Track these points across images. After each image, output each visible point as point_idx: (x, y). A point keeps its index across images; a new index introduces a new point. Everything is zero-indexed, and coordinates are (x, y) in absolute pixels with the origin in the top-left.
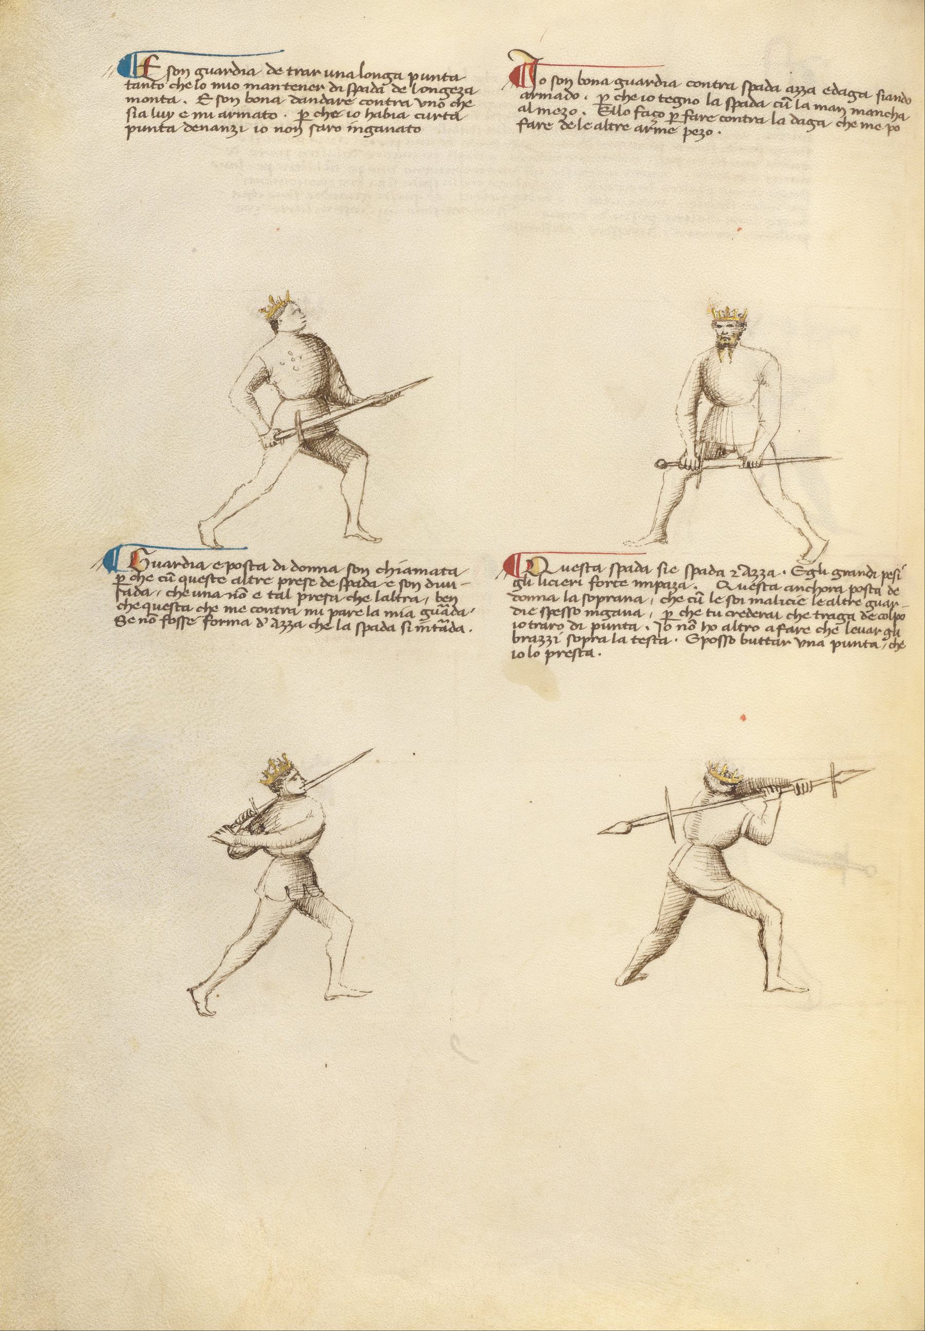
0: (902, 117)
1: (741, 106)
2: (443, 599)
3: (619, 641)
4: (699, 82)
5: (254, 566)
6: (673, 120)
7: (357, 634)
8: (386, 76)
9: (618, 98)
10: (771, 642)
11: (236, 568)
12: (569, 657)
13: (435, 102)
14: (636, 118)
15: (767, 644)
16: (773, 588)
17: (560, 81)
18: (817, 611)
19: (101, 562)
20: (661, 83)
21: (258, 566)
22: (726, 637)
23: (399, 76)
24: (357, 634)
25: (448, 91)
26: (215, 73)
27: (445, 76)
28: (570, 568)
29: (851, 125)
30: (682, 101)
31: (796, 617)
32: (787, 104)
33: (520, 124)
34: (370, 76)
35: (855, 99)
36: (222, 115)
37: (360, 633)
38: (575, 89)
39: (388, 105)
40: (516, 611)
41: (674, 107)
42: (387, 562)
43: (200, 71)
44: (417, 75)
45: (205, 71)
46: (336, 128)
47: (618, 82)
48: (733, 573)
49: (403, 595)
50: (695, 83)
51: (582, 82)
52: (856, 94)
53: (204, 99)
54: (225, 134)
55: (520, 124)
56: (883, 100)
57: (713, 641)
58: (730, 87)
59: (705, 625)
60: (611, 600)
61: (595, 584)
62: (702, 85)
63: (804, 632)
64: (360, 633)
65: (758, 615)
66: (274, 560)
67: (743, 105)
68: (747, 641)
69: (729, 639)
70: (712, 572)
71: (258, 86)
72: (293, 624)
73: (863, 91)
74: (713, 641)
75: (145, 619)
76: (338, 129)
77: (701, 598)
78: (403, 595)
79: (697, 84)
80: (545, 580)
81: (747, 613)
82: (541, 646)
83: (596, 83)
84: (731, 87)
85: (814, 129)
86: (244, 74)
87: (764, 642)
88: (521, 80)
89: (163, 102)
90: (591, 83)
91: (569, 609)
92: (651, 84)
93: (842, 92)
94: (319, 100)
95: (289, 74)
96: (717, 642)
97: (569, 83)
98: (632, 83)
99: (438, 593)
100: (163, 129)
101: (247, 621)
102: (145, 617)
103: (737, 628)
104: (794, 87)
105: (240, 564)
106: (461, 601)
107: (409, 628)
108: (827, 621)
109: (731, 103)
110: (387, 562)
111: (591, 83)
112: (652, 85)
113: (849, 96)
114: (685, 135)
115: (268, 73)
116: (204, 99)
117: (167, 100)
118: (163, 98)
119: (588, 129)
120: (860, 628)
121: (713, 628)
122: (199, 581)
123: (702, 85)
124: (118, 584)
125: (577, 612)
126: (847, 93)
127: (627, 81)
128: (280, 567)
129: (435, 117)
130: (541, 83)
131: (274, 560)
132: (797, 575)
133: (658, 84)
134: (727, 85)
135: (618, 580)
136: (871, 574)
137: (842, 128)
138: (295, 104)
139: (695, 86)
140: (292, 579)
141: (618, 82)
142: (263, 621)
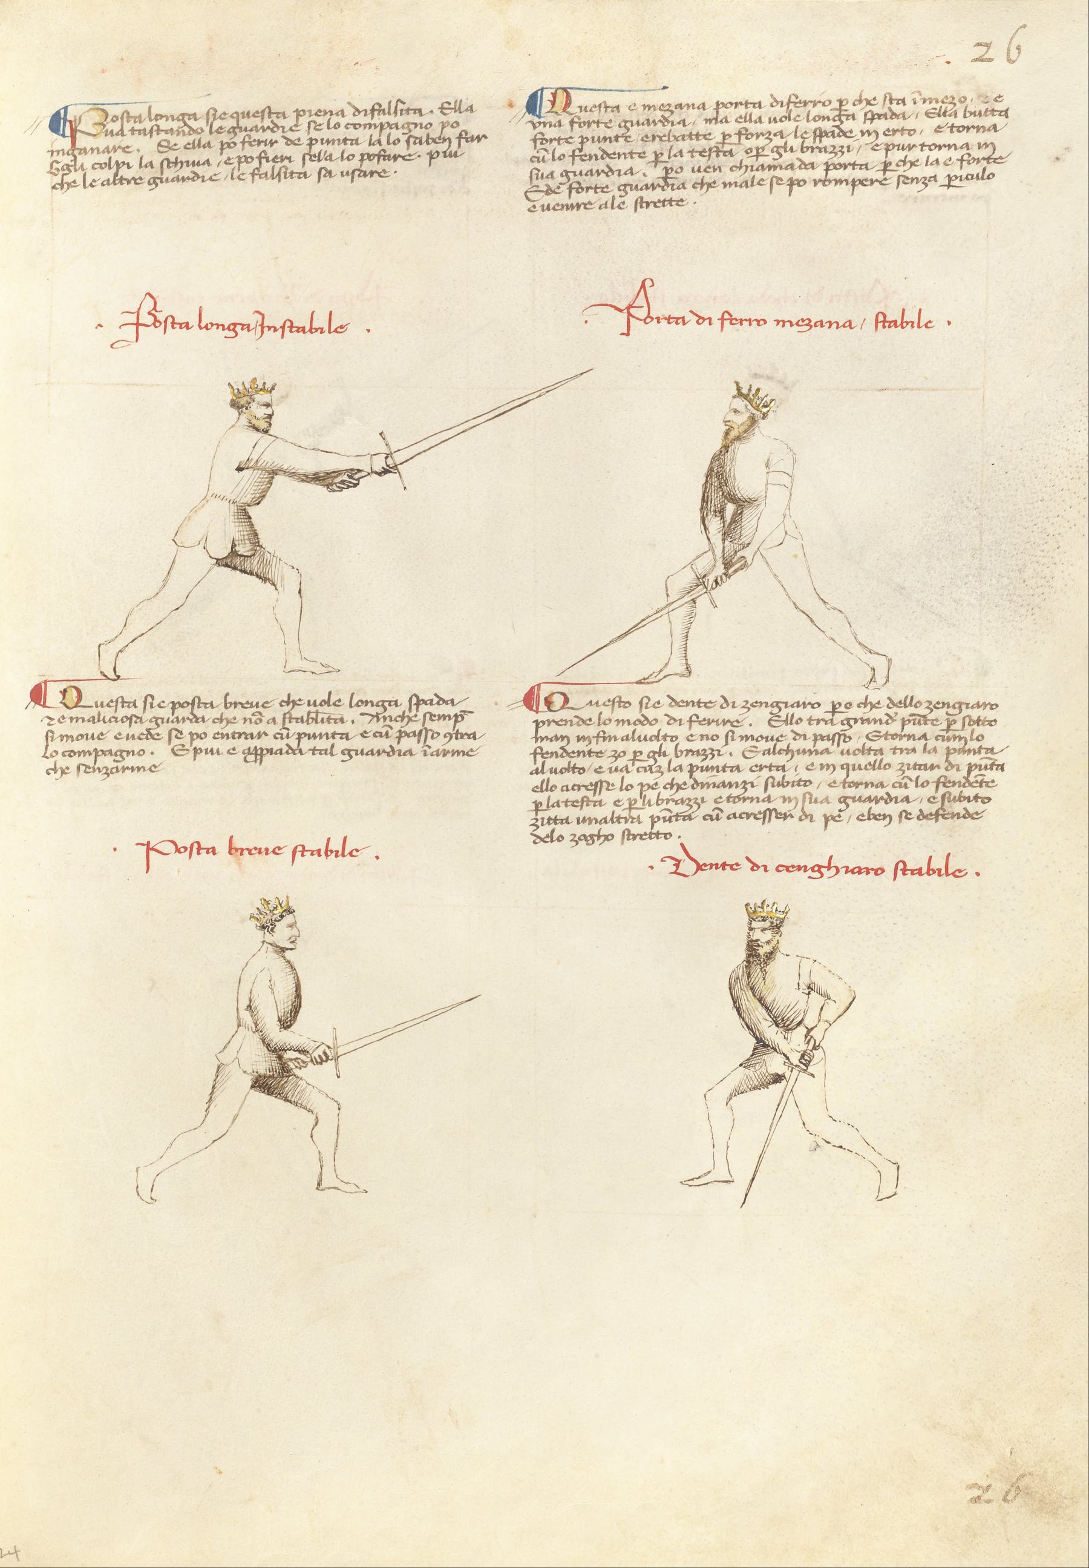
0: (991, 723)
1: (823, 740)
3: (146, 166)
4: (962, 126)
6: (951, 184)
9: (50, 771)
10: (775, 768)
12: (758, 819)
13: (556, 752)
16: (922, 767)
20: (698, 785)
23: (194, 116)
28: (851, 751)
30: (238, 328)
31: (62, 188)
32: (387, 733)
33: (535, 140)
35: (351, 757)
39: (556, 824)
42: (289, 695)
43: (235, 327)
44: (200, 749)
45: (572, 174)
47: (564, 174)
52: (352, 753)
55: (535, 754)
56: (773, 786)
57: (729, 105)
59: (149, 135)
62: (937, 148)
65: (560, 207)
67: (825, 738)
73: (191, 111)
75: (250, 720)
76: (668, 836)
79: (961, 129)
83: (982, 129)
88: (61, 129)
90: (976, 162)
92: (658, 188)
93: (428, 702)
94: (559, 754)
96: (190, 706)
98: (362, 753)
100: (175, 326)
104: (681, 323)
108: (926, 745)
110: (289, 695)
112: (882, 802)
117: (775, 768)
118: (699, 702)
121: (610, 838)
123: (937, 148)
127: (163, 719)
128: (806, 816)
135: (672, 815)
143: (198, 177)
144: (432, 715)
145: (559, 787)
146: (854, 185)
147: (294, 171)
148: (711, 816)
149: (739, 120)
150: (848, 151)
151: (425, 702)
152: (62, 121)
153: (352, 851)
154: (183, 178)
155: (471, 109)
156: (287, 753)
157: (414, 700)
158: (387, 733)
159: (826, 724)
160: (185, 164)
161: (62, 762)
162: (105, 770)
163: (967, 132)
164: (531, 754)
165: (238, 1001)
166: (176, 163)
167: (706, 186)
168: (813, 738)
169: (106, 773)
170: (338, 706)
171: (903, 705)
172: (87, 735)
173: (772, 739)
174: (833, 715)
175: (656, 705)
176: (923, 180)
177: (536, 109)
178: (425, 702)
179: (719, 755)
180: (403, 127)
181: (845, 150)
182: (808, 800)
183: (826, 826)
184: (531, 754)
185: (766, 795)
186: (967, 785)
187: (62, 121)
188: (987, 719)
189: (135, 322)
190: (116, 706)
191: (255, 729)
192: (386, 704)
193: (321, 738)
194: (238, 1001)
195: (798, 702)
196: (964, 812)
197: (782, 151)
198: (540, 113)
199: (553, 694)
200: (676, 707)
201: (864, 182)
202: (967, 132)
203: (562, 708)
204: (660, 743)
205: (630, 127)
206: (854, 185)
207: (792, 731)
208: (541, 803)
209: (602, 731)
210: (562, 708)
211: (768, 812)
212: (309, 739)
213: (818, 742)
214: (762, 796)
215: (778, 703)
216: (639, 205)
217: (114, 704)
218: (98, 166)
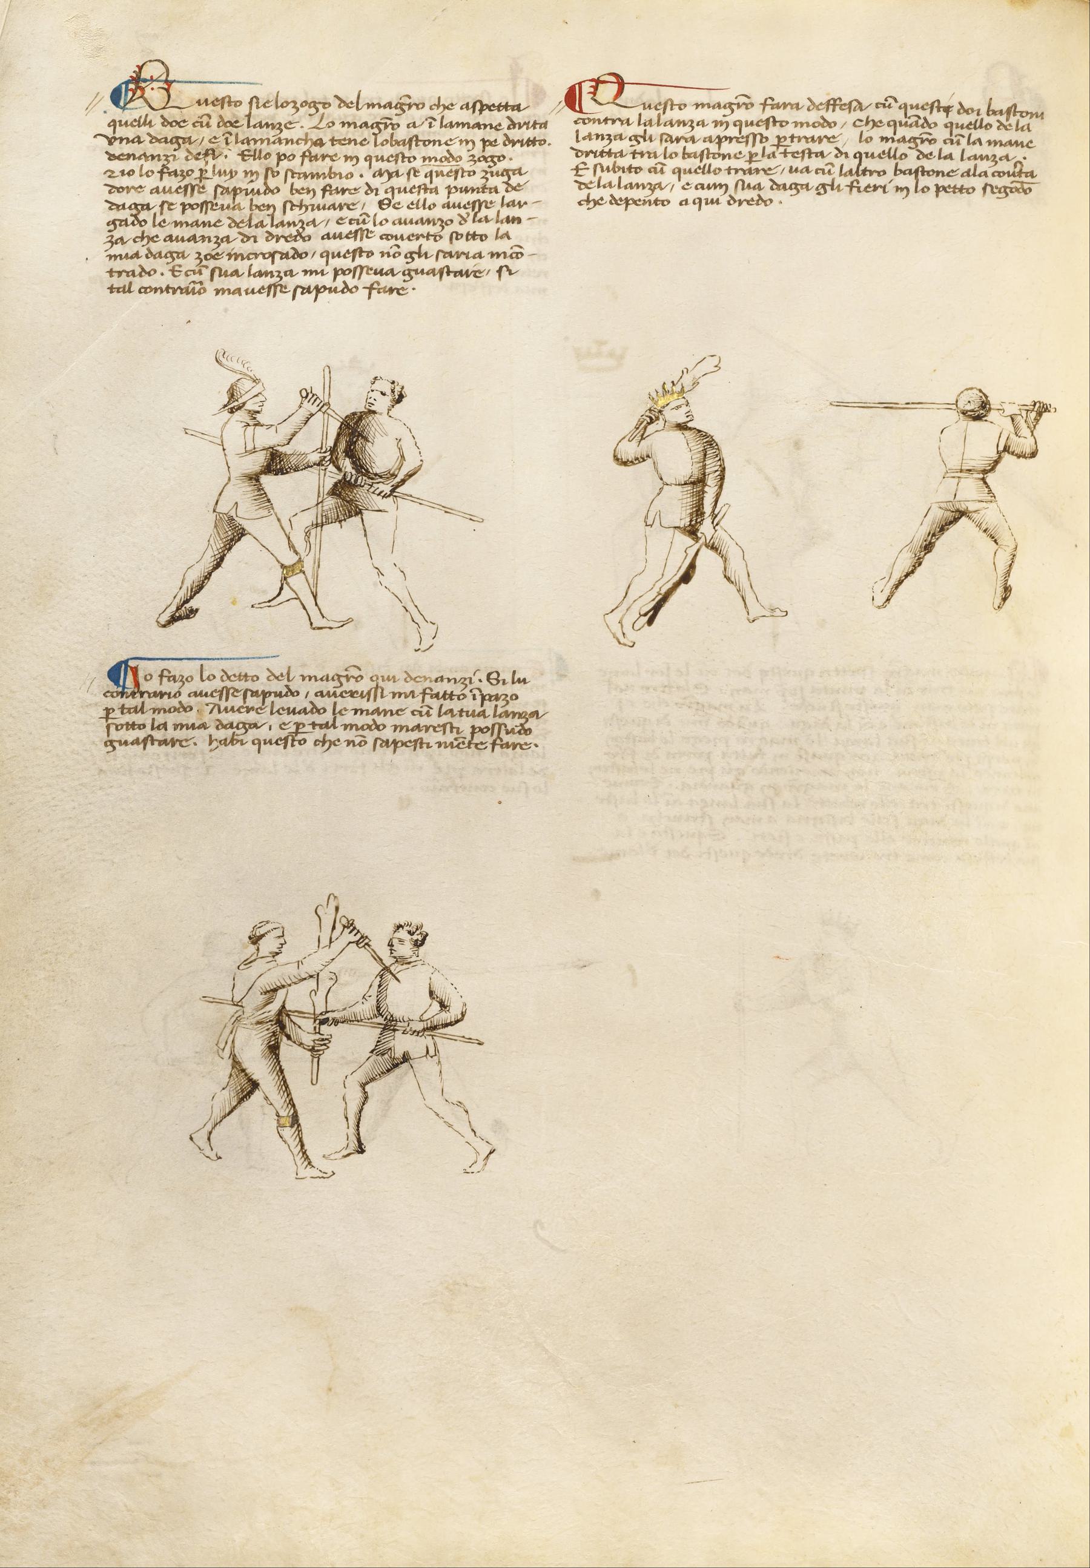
2: (297, 191)
8: (169, 255)
10: (479, 237)
19: (563, 103)
21: (455, 273)
25: (139, 207)
29: (596, 203)
32: (829, 171)
38: (766, 194)
40: (112, 189)
41: (724, 116)
48: (197, 255)
49: (475, 741)
51: (991, 113)
53: (581, 169)
54: (789, 192)
56: (220, 276)
57: (195, 207)
63: (349, 208)
64: (537, 133)
71: (121, 259)
74: (195, 207)
76: (749, 106)
77: (364, 220)
78: (475, 741)
81: (296, 236)
89: (656, 205)
91: (755, 136)
97: (470, 143)
99: (897, 164)
101: (759, 184)
103: (860, 172)
105: (197, 204)
106: (101, 664)
109: (478, 106)
111: (935, 174)
116: (581, 169)
118: (168, 288)
119: (289, 241)
120: (596, 151)
124: (107, 718)
126: (163, 255)
129: (875, 188)
136: (257, 742)
137: (585, 206)
140: (164, 692)
142: (465, 216)
143: (735, 201)
146: (627, 204)
147: (431, 233)
148: (420, 712)
149: (411, 206)
153: (855, 122)
154: (519, 203)
155: (580, 203)
156: (133, 224)
158: (829, 171)
159: (622, 124)
160: (310, 208)
161: (595, 194)
162: (300, 224)
165: (304, 608)
166: (301, 206)
168: (935, 189)
169: (650, 189)
170: (284, 729)
172: (313, 210)
175: (1030, 145)
176: (278, 126)
180: (130, 207)
182: (254, 105)
185: (482, 709)
192: (175, 255)
193: (709, 185)
194: (304, 608)
195: (631, 184)
196: (758, 198)
197: (415, 256)
201: (638, 202)
206: (627, 204)
211: (497, 727)
213: (475, 735)
214: (478, 709)
216: (418, 745)
218: (581, 121)
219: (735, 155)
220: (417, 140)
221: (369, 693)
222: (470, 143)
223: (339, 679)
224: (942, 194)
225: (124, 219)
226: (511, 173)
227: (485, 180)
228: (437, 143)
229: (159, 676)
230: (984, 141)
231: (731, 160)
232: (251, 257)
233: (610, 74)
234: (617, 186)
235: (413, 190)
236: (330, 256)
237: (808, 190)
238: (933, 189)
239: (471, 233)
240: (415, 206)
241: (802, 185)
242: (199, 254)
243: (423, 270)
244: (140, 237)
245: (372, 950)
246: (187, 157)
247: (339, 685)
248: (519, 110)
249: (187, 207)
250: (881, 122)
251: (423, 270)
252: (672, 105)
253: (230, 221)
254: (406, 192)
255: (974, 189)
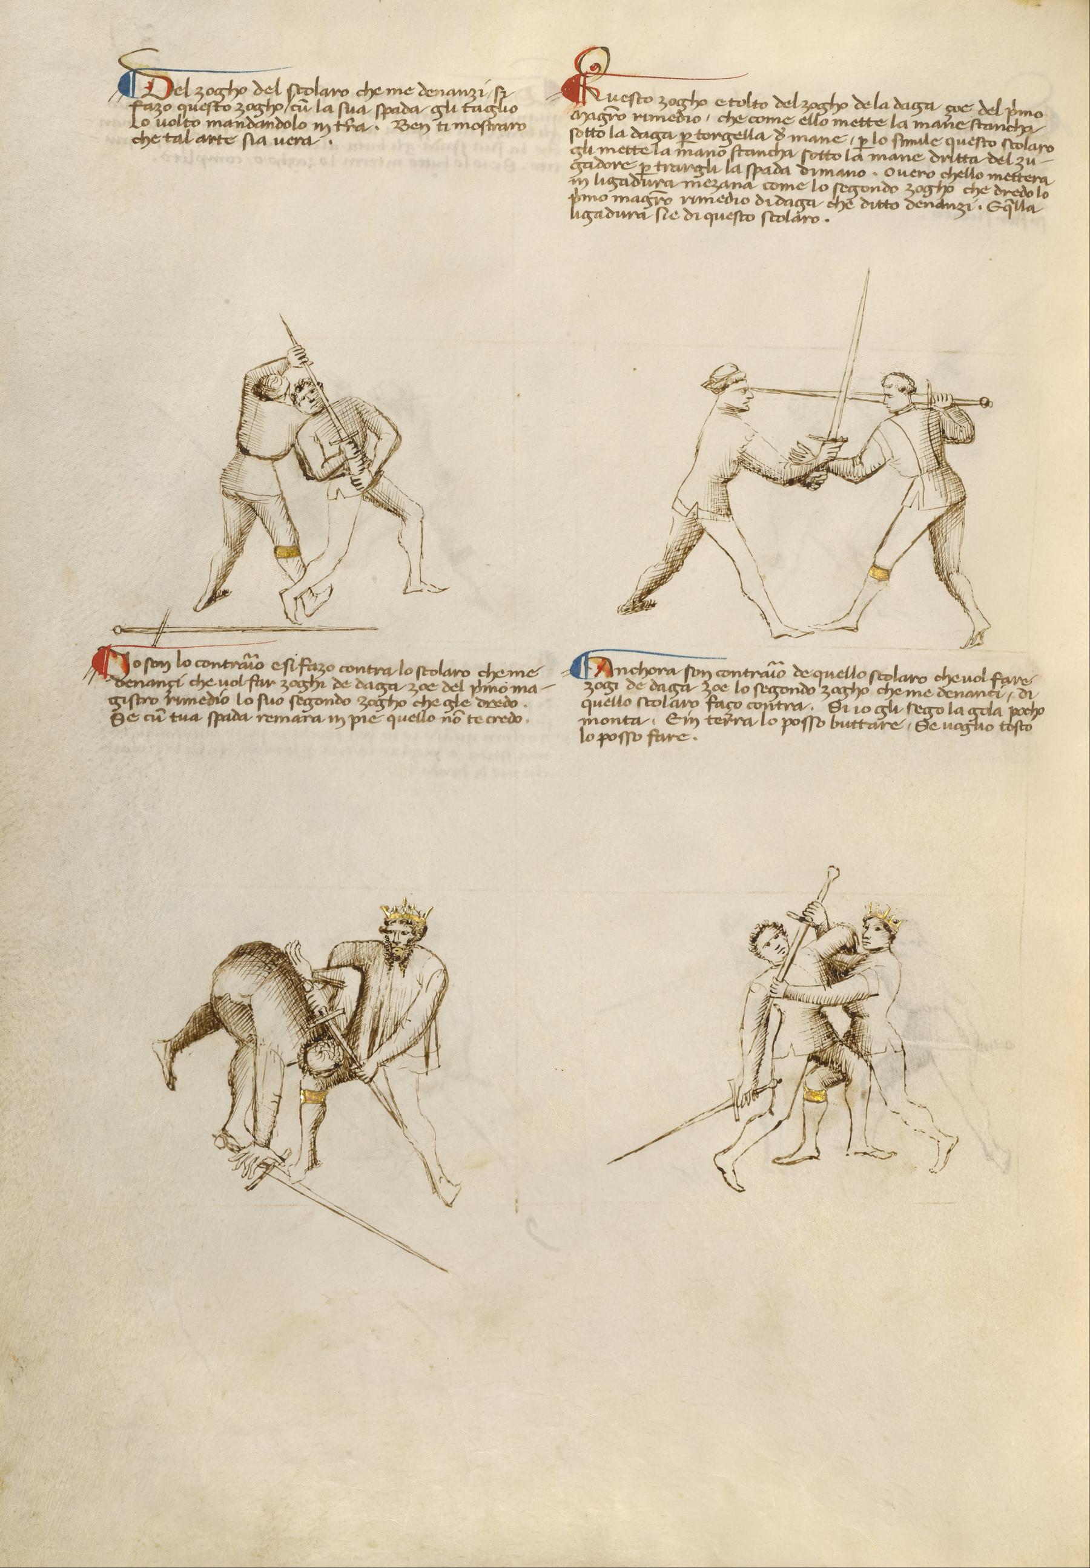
5: (743, 151)
6: (645, 172)
7: (209, 724)
11: (794, 725)
14: (650, 744)
15: (861, 728)
17: (696, 673)
18: (168, 134)
20: (732, 200)
22: (628, 734)
24: (209, 724)
26: (610, 164)
27: (226, 662)
31: (728, 121)
34: (277, 701)
36: (856, 158)
37: (213, 723)
43: (116, 701)
46: (692, 703)
47: (447, 703)
50: (758, 118)
56: (252, 144)
58: (747, 722)
60: (740, 722)
61: (254, 683)
64: (213, 723)
65: (294, 142)
66: (775, 97)
68: (838, 724)
69: (815, 721)
70: (406, 110)
72: (913, 188)
80: (578, 212)
82: (833, 96)
84: (344, 92)
85: (920, 112)
86: (525, 691)
87: (857, 725)
95: (469, 722)
97: (341, 721)
102: (219, 695)
107: (292, 665)
113: (599, 120)
114: (784, 727)
115: (420, 94)
122: (728, 218)
125: (821, 724)
130: (135, 666)
131: (775, 97)
132: (674, 724)
133: (729, 200)
134: (384, 670)
136: (392, 719)
138: (505, 724)
139: (203, 666)
141: (447, 703)
144: (984, 141)
145: (193, 663)
150: (481, 95)
151: (392, 111)
152: (581, 89)
157: (381, 109)
162: (472, 92)
163: (713, 139)
164: (130, 106)
167: (201, 683)
171: (742, 137)
173: (685, 152)
174: (861, 151)
175: (408, 92)
177: (129, 91)
178: (392, 111)
179: (969, 210)
181: (478, 94)
183: (784, 730)
184: (130, 106)
186: (251, 125)
187: (581, 89)
188: (831, 152)
189: (228, 87)
190: (735, 219)
191: (856, 166)
198: (133, 95)
199: (223, 100)
200: (610, 734)
202: (713, 139)
203: (168, 94)
204: (294, 113)
205: (680, 691)
207: (444, 682)
208: (866, 140)
209: (890, 169)
210: (168, 94)
212: (872, 208)
215: (802, 201)
217: (733, 217)
219: (925, 694)
220: (1022, 725)
221: (286, 664)
222: (341, 721)
223: (304, 685)
224: (790, 728)
225: (178, 135)
226: (805, 203)
227: (1019, 167)
228: (623, 671)
229: (171, 717)
230: (985, 174)
231: (602, 708)
232: (291, 142)
233: (674, 724)
234: (760, 722)
235: (841, 675)
236: (396, 721)
237: (751, 725)
238: (781, 723)
239: (866, 119)
240: (611, 703)
241: (809, 201)
242: (1022, 159)
243: (186, 716)
244: (884, 689)
245: (348, 669)
246: (856, 105)
247: (610, 691)
248: (639, 723)
249: (789, 722)
250: (379, 89)
251: (186, 716)
252: (138, 699)
253: (907, 203)
254: (970, 681)
255: (349, 700)
